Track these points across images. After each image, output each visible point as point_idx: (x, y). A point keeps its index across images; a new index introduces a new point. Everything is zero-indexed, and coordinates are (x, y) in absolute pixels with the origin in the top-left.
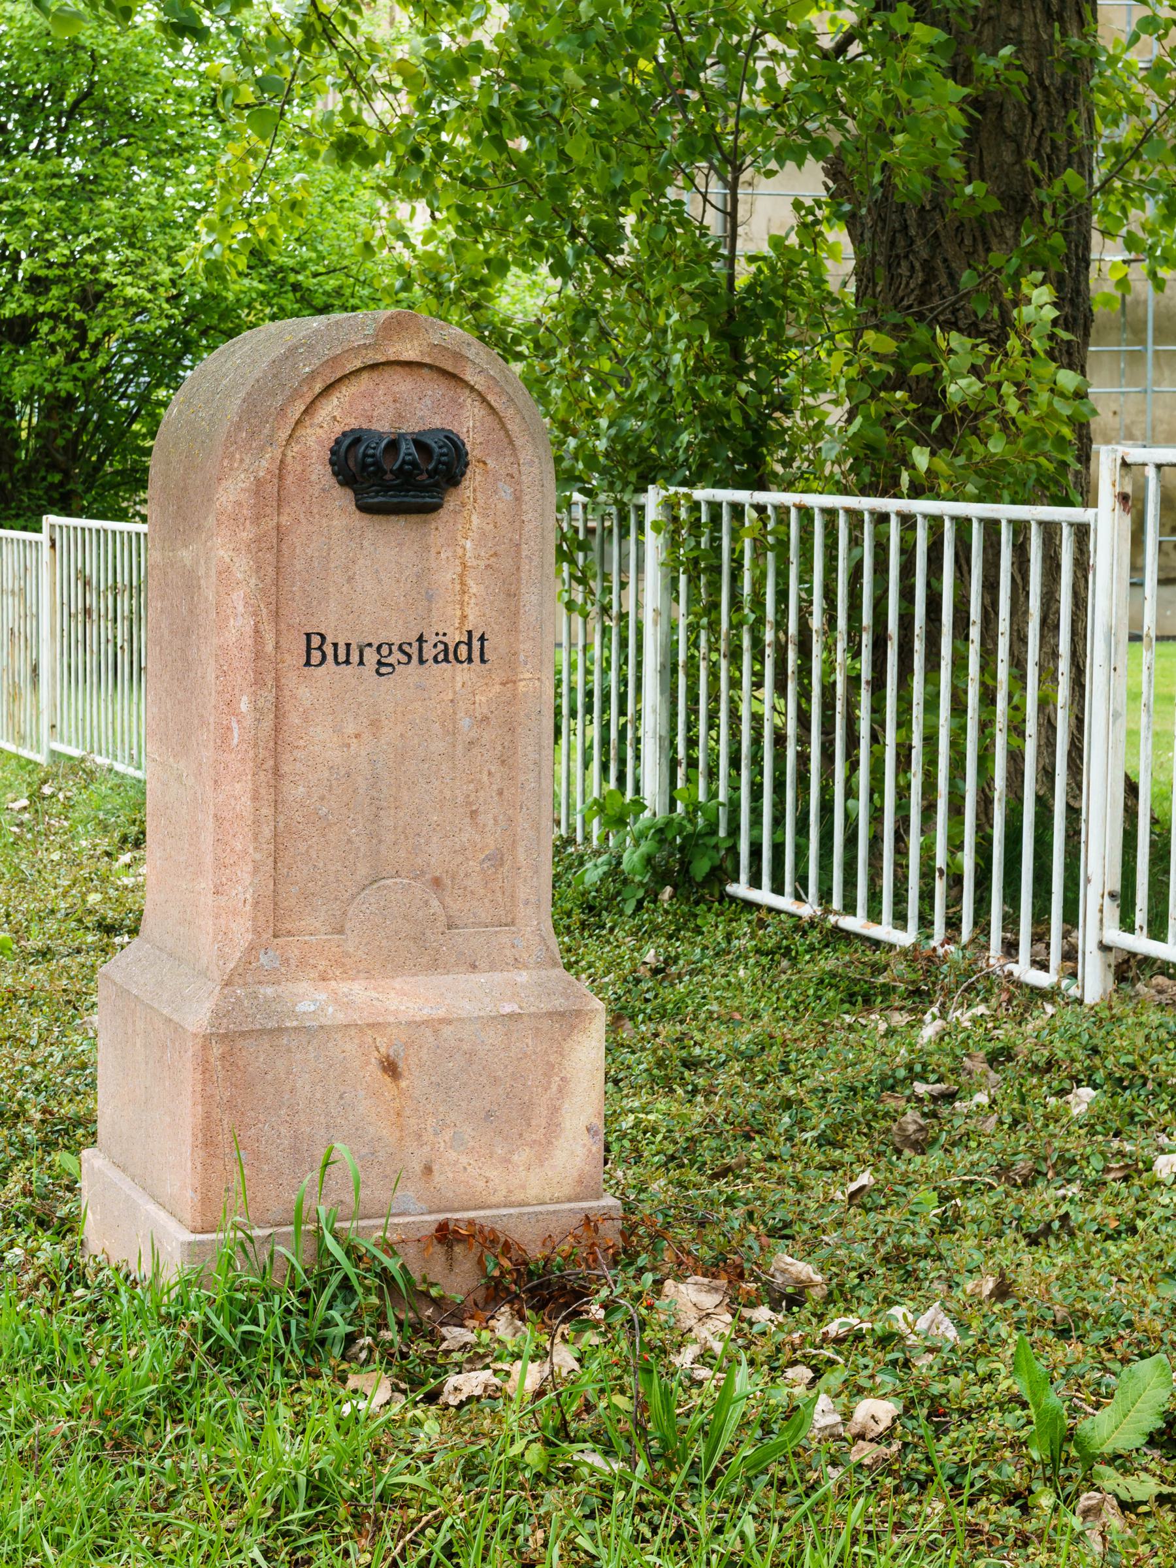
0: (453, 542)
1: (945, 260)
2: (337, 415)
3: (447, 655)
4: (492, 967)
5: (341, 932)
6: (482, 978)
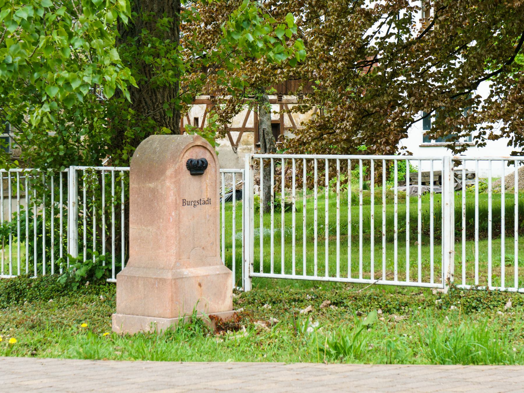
0: (205, 181)
1: (144, 98)
2: (188, 156)
3: (205, 203)
4: (213, 265)
5: (189, 258)
6: (211, 267)
